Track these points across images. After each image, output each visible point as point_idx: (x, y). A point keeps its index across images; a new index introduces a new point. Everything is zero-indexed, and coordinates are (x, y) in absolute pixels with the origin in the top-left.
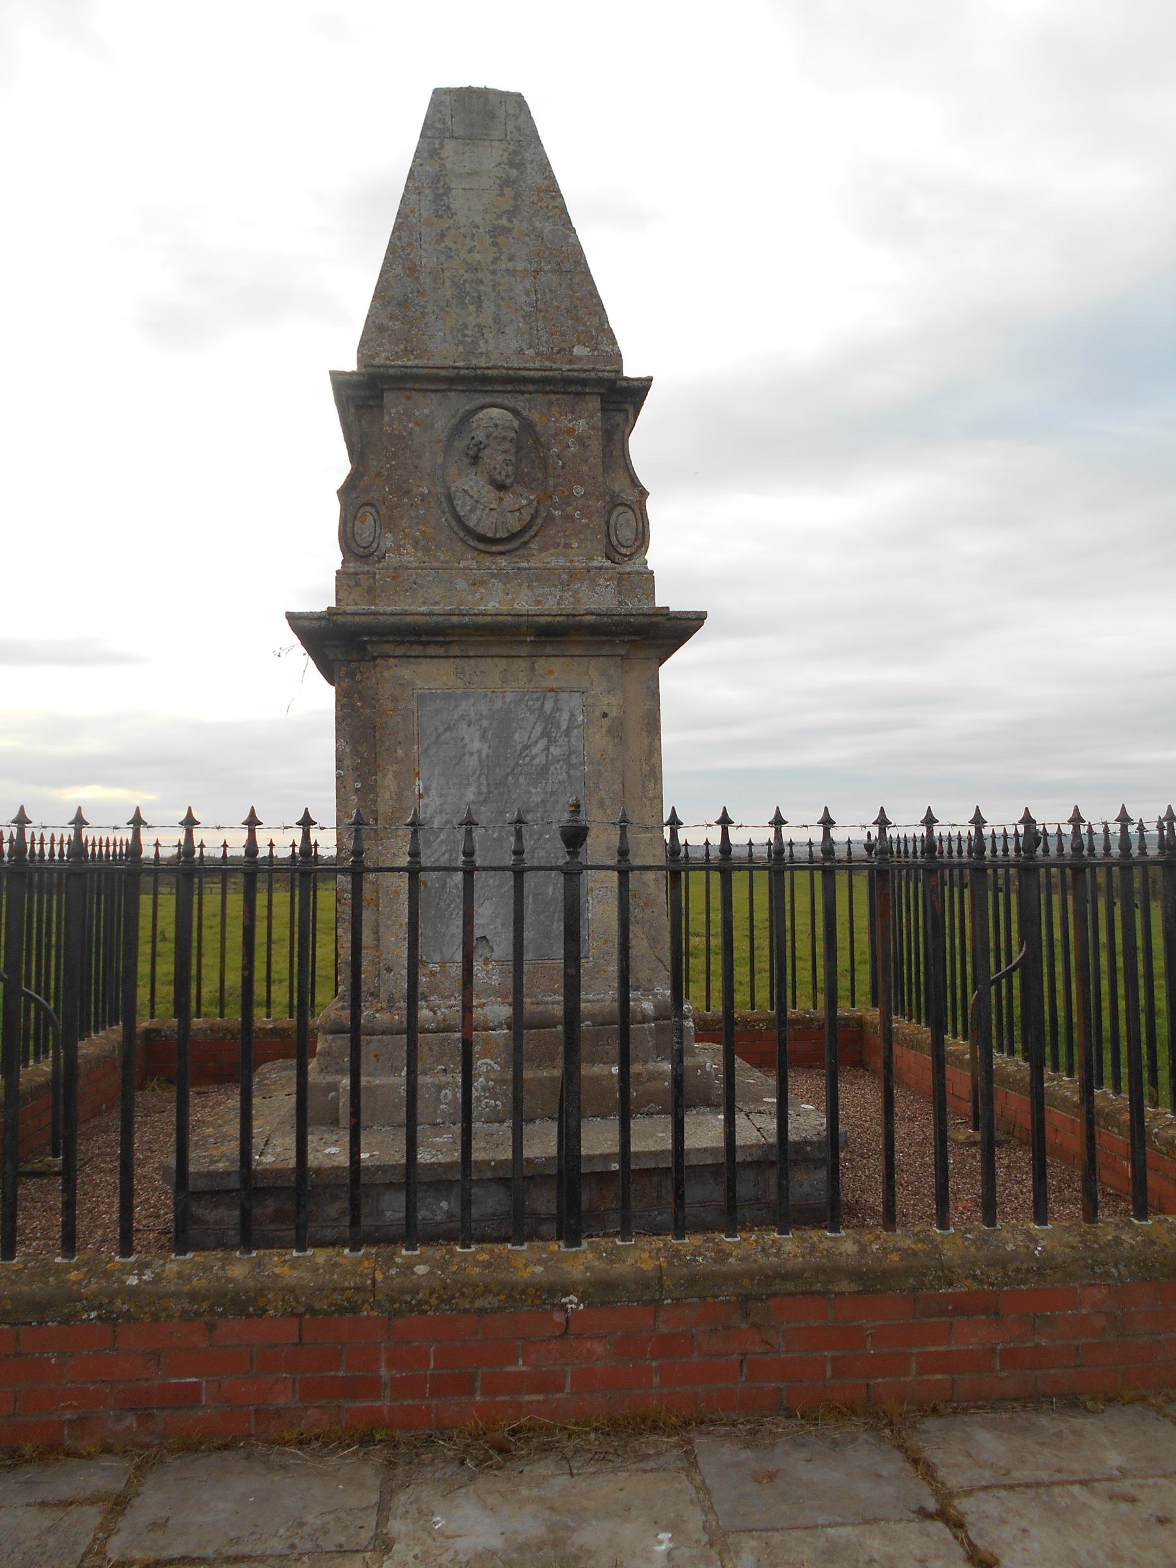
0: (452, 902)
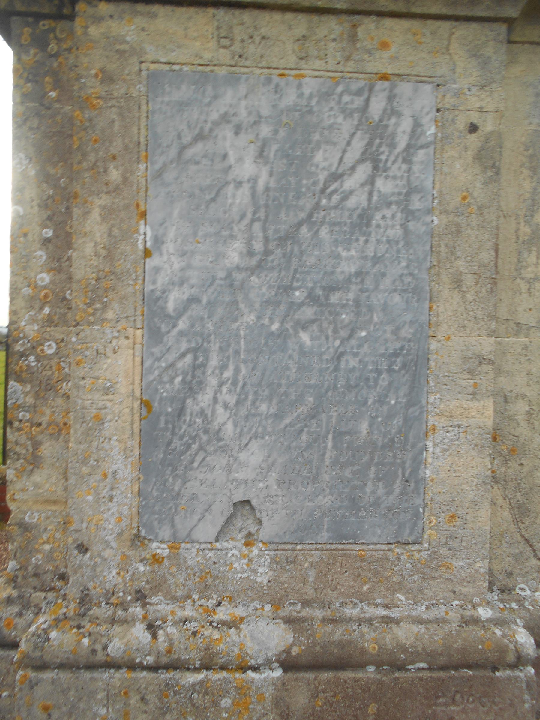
0: (194, 438)
